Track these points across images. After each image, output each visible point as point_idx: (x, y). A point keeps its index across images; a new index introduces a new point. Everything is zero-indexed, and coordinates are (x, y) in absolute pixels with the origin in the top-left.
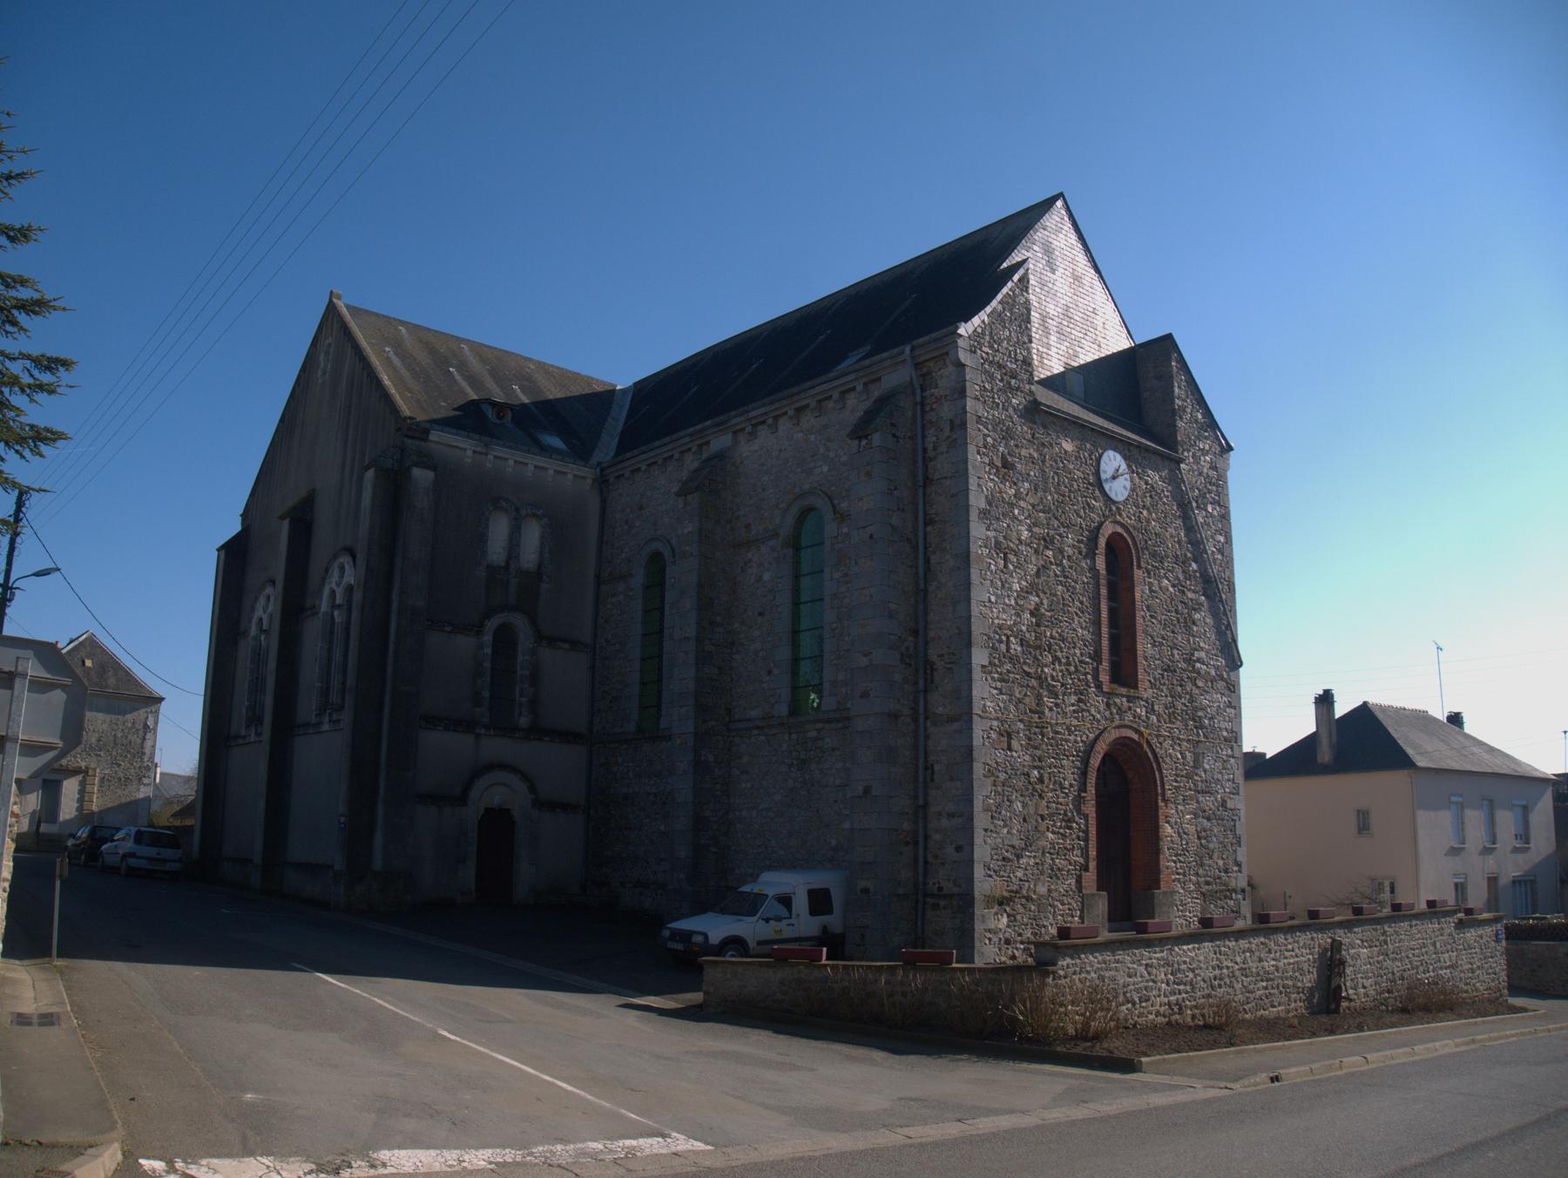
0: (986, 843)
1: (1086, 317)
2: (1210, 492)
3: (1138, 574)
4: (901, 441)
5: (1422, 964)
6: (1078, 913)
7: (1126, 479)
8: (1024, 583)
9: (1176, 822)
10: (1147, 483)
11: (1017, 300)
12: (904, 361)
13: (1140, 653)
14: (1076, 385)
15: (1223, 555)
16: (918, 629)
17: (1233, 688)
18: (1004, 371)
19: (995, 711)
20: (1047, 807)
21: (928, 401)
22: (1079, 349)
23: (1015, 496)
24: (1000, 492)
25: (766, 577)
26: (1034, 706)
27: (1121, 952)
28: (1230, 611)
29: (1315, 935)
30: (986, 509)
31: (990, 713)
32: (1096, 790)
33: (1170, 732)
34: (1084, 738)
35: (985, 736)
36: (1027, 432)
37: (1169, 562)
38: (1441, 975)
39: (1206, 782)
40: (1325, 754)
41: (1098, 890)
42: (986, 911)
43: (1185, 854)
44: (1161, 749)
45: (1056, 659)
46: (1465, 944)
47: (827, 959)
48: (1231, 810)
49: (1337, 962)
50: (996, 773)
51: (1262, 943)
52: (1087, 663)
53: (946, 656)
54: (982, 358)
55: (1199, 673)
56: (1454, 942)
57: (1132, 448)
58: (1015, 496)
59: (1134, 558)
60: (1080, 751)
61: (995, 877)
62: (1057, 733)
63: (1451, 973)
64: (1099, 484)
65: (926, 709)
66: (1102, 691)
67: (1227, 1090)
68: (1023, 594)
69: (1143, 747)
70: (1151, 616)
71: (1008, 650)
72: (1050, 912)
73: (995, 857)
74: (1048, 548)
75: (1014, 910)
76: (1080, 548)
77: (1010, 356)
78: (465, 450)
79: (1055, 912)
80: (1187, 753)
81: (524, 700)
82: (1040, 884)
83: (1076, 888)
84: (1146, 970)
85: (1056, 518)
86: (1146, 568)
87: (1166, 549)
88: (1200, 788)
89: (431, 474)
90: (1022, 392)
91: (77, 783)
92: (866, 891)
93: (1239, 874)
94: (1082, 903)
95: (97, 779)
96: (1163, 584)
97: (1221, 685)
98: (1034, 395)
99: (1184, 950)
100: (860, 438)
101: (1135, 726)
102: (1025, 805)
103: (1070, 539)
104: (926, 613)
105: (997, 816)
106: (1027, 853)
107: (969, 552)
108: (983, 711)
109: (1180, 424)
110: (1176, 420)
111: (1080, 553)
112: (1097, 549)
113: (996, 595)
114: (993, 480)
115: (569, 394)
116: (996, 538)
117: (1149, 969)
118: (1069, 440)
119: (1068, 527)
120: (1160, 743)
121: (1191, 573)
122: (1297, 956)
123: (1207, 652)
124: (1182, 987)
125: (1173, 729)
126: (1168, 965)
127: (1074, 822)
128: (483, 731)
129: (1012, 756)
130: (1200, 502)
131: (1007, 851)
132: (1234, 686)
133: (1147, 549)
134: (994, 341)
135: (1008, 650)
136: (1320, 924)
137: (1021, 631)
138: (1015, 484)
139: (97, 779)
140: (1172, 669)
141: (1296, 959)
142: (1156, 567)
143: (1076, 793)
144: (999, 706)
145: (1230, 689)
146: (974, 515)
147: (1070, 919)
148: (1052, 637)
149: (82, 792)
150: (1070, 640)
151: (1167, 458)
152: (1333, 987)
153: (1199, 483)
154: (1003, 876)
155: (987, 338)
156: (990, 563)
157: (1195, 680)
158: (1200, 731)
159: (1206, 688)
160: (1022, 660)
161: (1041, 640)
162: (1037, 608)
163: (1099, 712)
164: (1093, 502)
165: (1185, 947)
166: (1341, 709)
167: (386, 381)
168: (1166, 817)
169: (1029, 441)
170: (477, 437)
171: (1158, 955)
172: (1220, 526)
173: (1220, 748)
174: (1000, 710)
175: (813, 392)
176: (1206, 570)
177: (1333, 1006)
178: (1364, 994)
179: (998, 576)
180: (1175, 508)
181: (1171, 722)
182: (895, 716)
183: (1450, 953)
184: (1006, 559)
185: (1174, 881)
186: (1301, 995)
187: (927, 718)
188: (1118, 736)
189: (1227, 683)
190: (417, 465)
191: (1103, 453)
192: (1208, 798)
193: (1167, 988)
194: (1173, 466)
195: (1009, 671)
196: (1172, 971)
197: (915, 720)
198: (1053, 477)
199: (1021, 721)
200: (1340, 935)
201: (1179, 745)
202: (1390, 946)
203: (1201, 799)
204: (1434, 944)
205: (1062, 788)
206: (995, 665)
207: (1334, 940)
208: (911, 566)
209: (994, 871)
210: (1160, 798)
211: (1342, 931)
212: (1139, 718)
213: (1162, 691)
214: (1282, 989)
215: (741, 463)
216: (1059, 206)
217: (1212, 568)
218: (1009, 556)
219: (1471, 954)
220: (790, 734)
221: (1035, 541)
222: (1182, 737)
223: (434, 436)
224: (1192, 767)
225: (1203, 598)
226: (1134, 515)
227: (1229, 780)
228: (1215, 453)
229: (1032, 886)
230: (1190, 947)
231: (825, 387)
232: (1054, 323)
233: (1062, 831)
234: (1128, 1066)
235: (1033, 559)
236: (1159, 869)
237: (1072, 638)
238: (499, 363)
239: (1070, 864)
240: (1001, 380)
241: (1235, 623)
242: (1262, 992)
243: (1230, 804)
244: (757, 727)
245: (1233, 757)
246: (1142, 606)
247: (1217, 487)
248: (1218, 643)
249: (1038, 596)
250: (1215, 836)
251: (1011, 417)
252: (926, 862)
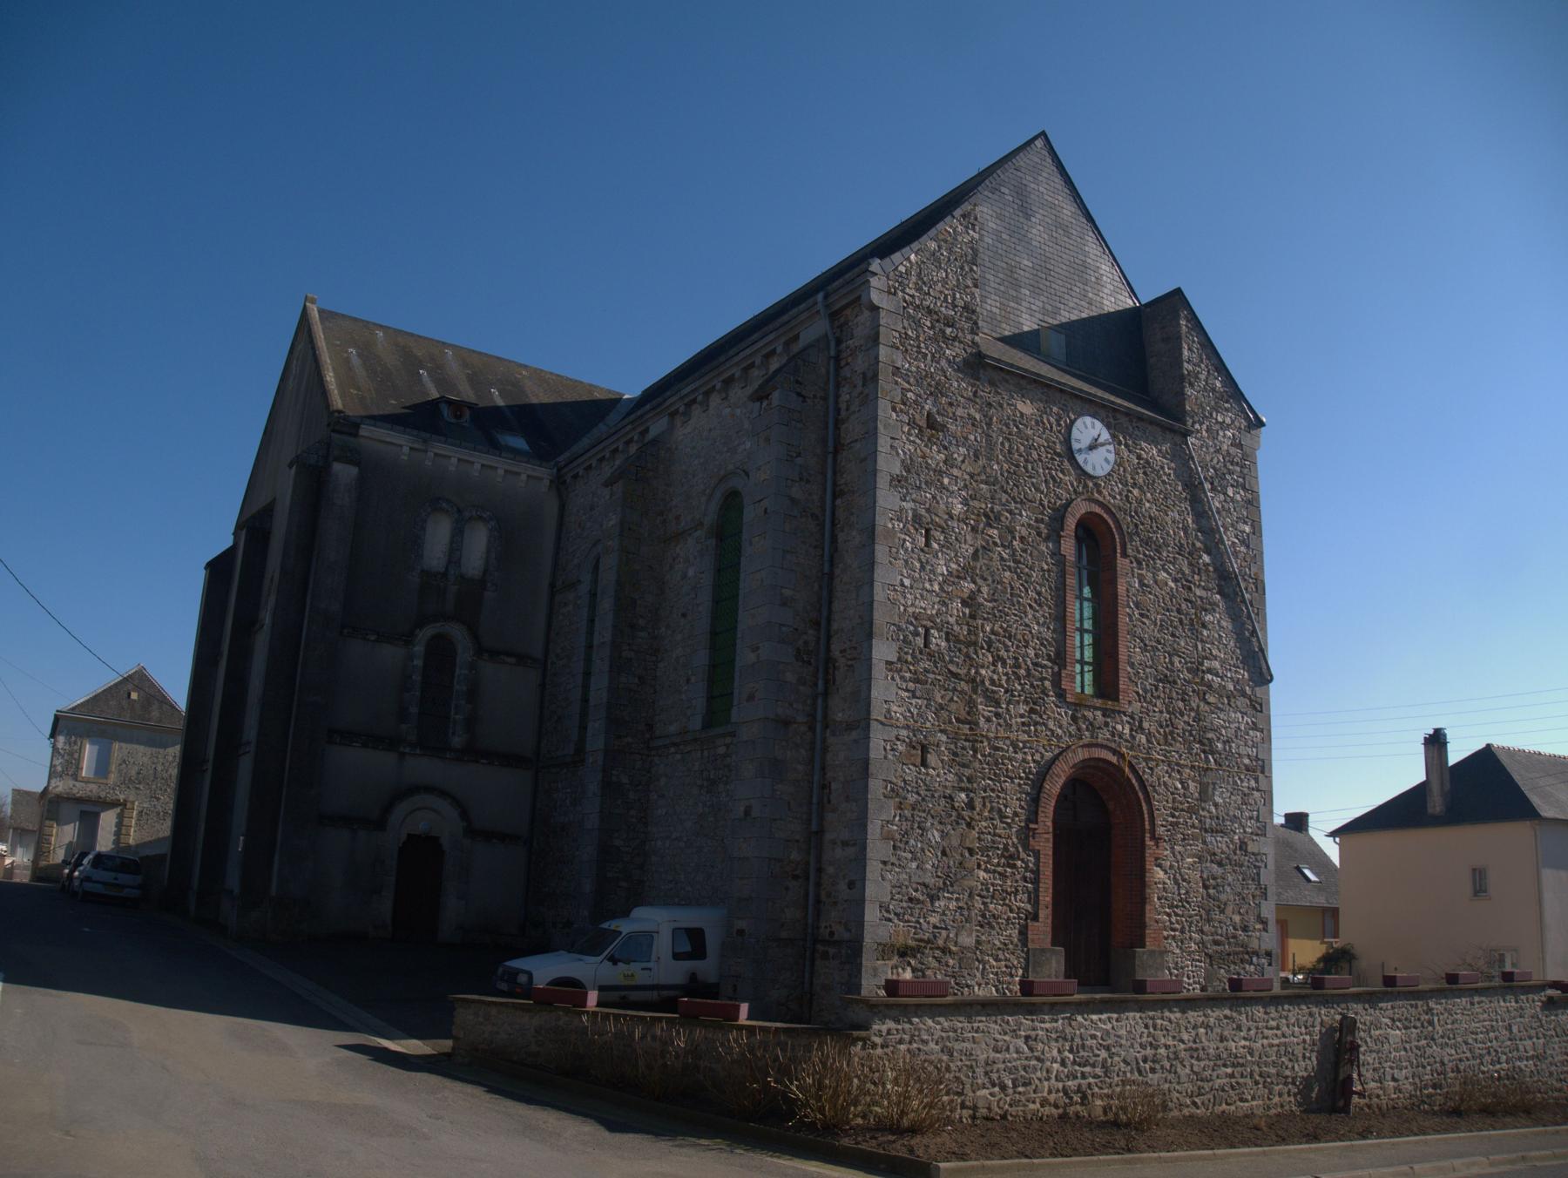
1: (1072, 271)
2: (1231, 473)
3: (1121, 562)
5: (1489, 1053)
6: (1020, 972)
8: (954, 566)
9: (1171, 867)
10: (1139, 457)
11: (960, 239)
12: (818, 312)
13: (1123, 657)
14: (1056, 344)
15: (1248, 547)
16: (821, 620)
17: (1259, 707)
18: (935, 317)
19: (905, 717)
20: (979, 838)
21: (844, 355)
24: (924, 457)
25: (691, 573)
26: (963, 715)
27: (984, 1019)
28: (1257, 614)
29: (1315, 1010)
30: (902, 476)
31: (897, 720)
33: (1165, 756)
34: (1037, 757)
35: (888, 747)
36: (966, 389)
38: (1519, 1067)
39: (1218, 818)
40: (1436, 805)
42: (879, 962)
43: (1183, 906)
44: (1151, 775)
46: (1558, 1030)
48: (1253, 854)
49: (1348, 1046)
51: (1226, 1017)
53: (849, 652)
54: (905, 301)
55: (1210, 686)
56: (1542, 1026)
57: (1118, 416)
59: (1118, 544)
60: (1030, 773)
61: (896, 921)
62: (997, 749)
63: (1536, 1065)
64: (1070, 454)
65: (825, 716)
68: (952, 579)
69: (1124, 772)
70: (1141, 615)
72: (977, 969)
73: (897, 896)
74: (991, 527)
75: (923, 964)
76: (1038, 528)
77: (946, 300)
78: (401, 446)
79: (984, 968)
80: (1190, 782)
82: (964, 932)
84: (1026, 1043)
85: (1006, 492)
86: (1135, 558)
89: (354, 471)
90: (960, 342)
91: (115, 816)
92: (741, 932)
93: (1264, 934)
94: (1027, 960)
95: (135, 813)
97: (1241, 702)
98: (978, 346)
99: (1092, 1021)
101: (1113, 745)
102: (944, 835)
103: (1025, 516)
105: (902, 846)
106: (946, 895)
107: (874, 525)
109: (1189, 391)
110: (1184, 387)
111: (1039, 534)
112: (1062, 530)
113: (913, 579)
114: (914, 442)
115: (560, 400)
116: (914, 510)
117: (1030, 1043)
119: (1022, 502)
120: (1151, 769)
121: (1201, 566)
122: (1284, 1036)
123: (1223, 662)
124: (1087, 1069)
125: (1170, 752)
126: (1065, 1039)
127: (1019, 859)
129: (928, 774)
130: (1216, 484)
131: (916, 891)
132: (1261, 705)
133: (1137, 534)
134: (924, 283)
137: (948, 623)
138: (945, 448)
139: (135, 813)
140: (1171, 679)
141: (1283, 1040)
142: (1150, 556)
143: (1023, 824)
144: (910, 711)
145: (1255, 708)
146: (882, 482)
148: (993, 632)
149: (119, 825)
150: (1020, 637)
153: (1215, 461)
154: (909, 921)
155: (914, 279)
156: (904, 540)
157: (1204, 694)
158: (1210, 757)
159: (1220, 705)
160: (947, 658)
163: (1060, 727)
164: (1061, 476)
165: (1095, 1017)
166: (1455, 754)
167: (330, 377)
168: (1157, 859)
169: (969, 399)
170: (415, 432)
171: (1047, 1025)
172: (1245, 513)
173: (1240, 778)
174: (913, 717)
175: (736, 359)
176: (1223, 564)
177: (1341, 1103)
178: (1395, 1088)
179: (914, 556)
180: (1180, 488)
181: (1166, 743)
184: (928, 536)
185: (1166, 938)
186: (1290, 1086)
189: (1251, 700)
190: (337, 459)
191: (1076, 419)
192: (1218, 839)
193: (1062, 1068)
194: (1178, 439)
195: (926, 670)
197: (812, 729)
198: (1002, 444)
201: (1179, 772)
202: (1438, 1027)
203: (1209, 839)
204: (1509, 1028)
205: (1002, 816)
206: (906, 662)
207: (1344, 1017)
208: (816, 547)
209: (895, 914)
210: (1148, 835)
212: (1120, 737)
213: (1155, 705)
214: (1258, 1078)
215: (676, 449)
216: (1039, 146)
217: (1231, 562)
218: (932, 532)
220: (702, 751)
221: (973, 517)
222: (1182, 762)
223: (365, 431)
224: (1197, 800)
225: (1218, 597)
226: (1120, 494)
227: (1251, 818)
228: (1240, 428)
229: (951, 935)
230: (1104, 1016)
231: (748, 351)
233: (999, 869)
236: (1145, 923)
237: (1024, 635)
238: (480, 367)
239: (1011, 911)
240: (932, 327)
241: (1264, 629)
243: (1251, 847)
244: (674, 744)
245: (1258, 790)
246: (1128, 601)
248: (1238, 651)
249: (974, 582)
250: (1229, 885)
251: (944, 372)
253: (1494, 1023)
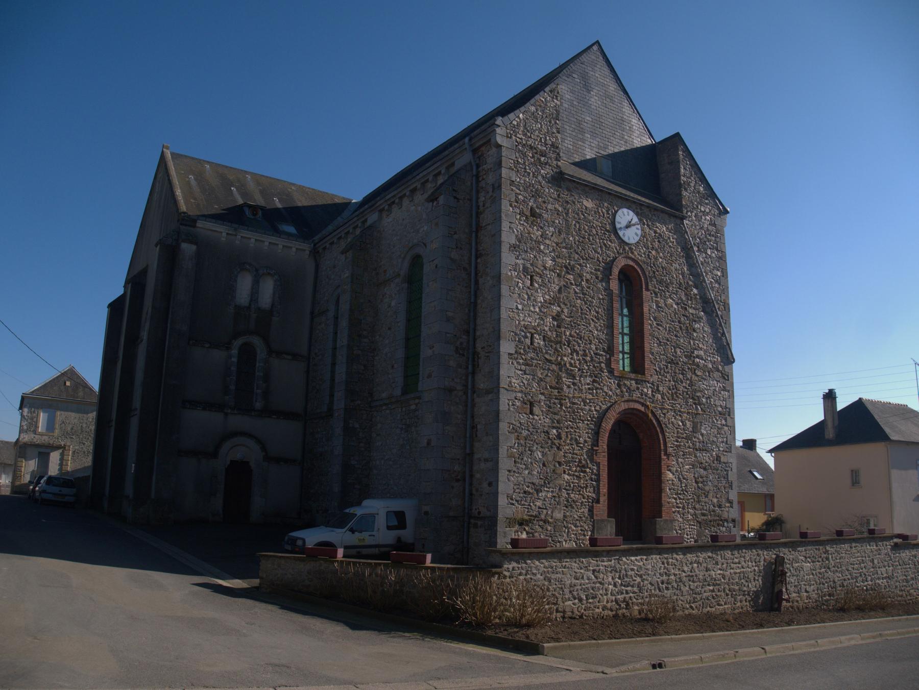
0: (509, 480)
2: (709, 241)
4: (461, 201)
5: (861, 575)
7: (637, 229)
8: (547, 297)
9: (677, 471)
10: (655, 232)
11: (549, 105)
12: (466, 149)
14: (606, 167)
15: (719, 284)
17: (727, 378)
18: (535, 151)
19: (520, 386)
20: (564, 456)
21: (481, 174)
22: (607, 143)
23: (541, 236)
24: (529, 233)
25: (393, 304)
26: (554, 384)
27: (569, 560)
29: (760, 552)
31: (515, 387)
32: (608, 446)
33: (672, 406)
34: (598, 408)
35: (511, 404)
37: (673, 287)
38: (878, 583)
39: (703, 442)
40: (830, 433)
41: (608, 517)
42: (507, 529)
43: (684, 494)
44: (664, 418)
45: (574, 351)
46: (900, 561)
47: (431, 563)
48: (724, 463)
50: (520, 430)
52: (601, 355)
54: (517, 142)
55: (698, 366)
56: (891, 560)
58: (541, 236)
60: (594, 417)
62: (574, 404)
63: (888, 582)
64: (615, 231)
66: (614, 375)
67: (602, 674)
69: (648, 416)
70: (657, 324)
71: (532, 343)
72: (565, 532)
73: (517, 490)
75: (533, 529)
77: (541, 141)
78: (221, 232)
79: (568, 532)
80: (687, 421)
81: (259, 391)
82: (556, 511)
83: (589, 515)
85: (577, 253)
87: (671, 278)
88: (697, 447)
89: (194, 247)
90: (550, 165)
92: (426, 513)
93: (731, 509)
94: (593, 526)
96: (669, 302)
97: (716, 375)
98: (560, 168)
99: (631, 560)
100: (432, 201)
102: (544, 454)
103: (589, 267)
104: (475, 319)
105: (519, 461)
108: (509, 386)
109: (684, 193)
111: (597, 278)
113: (523, 305)
114: (523, 224)
116: (524, 265)
117: (596, 574)
118: (590, 200)
120: (664, 414)
121: (692, 296)
122: (743, 567)
123: (705, 351)
124: (629, 588)
126: (616, 571)
127: (588, 467)
128: (229, 411)
129: (534, 419)
130: (700, 247)
132: (728, 376)
133: (655, 277)
134: (528, 131)
135: (532, 343)
136: (765, 544)
137: (544, 330)
138: (542, 228)
140: (675, 362)
143: (590, 447)
144: (523, 382)
146: (505, 248)
147: (582, 537)
148: (571, 335)
149: (62, 459)
150: (586, 338)
151: (672, 215)
152: (776, 590)
153: (700, 234)
154: (524, 505)
155: (522, 129)
156: (518, 282)
157: (695, 370)
161: (561, 337)
162: (558, 314)
164: (610, 243)
165: (633, 558)
166: (841, 405)
167: (178, 193)
168: (668, 466)
169: (555, 199)
170: (230, 224)
171: (606, 563)
173: (716, 419)
176: (705, 294)
178: (807, 597)
180: (679, 250)
181: (673, 399)
182: (450, 390)
183: (887, 568)
184: (532, 280)
185: (674, 512)
186: (747, 596)
187: (474, 392)
188: (627, 407)
189: (722, 374)
190: (184, 241)
191: (618, 210)
192: (704, 454)
193: (614, 588)
194: (678, 221)
195: (532, 358)
196: (620, 576)
197: (466, 393)
198: (575, 225)
199: (542, 394)
200: (786, 553)
201: (680, 415)
202: (831, 561)
203: (698, 455)
204: (872, 561)
205: (578, 443)
206: (520, 353)
207: (778, 556)
209: (516, 501)
210: (663, 453)
211: (787, 550)
212: (646, 396)
214: (728, 592)
215: (384, 231)
218: (535, 277)
219: (906, 568)
221: (558, 268)
222: (682, 410)
223: (200, 224)
224: (691, 432)
225: (702, 313)
226: (644, 254)
227: (723, 442)
228: (715, 215)
230: (638, 558)
231: (425, 173)
232: (589, 126)
233: (576, 474)
234: (532, 649)
235: (556, 280)
236: (662, 503)
237: (589, 337)
238: (267, 185)
239: (584, 498)
241: (729, 332)
242: (709, 594)
243: (723, 459)
245: (727, 426)
247: (715, 237)
248: (714, 345)
250: (710, 481)
252: (471, 494)
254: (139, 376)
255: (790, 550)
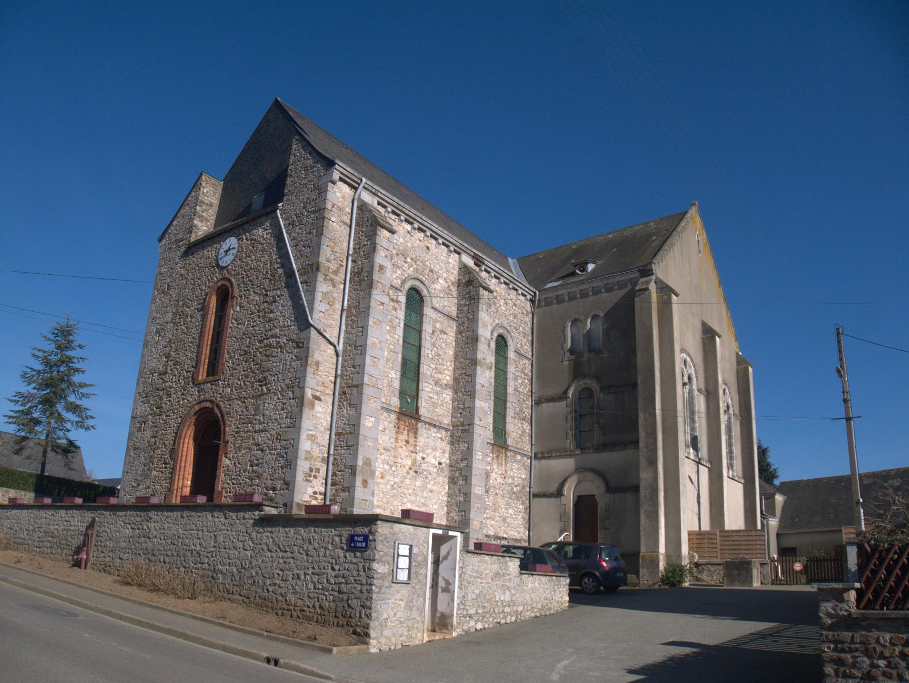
43: (237, 479)
253: (200, 533)
254: (724, 438)
255: (112, 514)
